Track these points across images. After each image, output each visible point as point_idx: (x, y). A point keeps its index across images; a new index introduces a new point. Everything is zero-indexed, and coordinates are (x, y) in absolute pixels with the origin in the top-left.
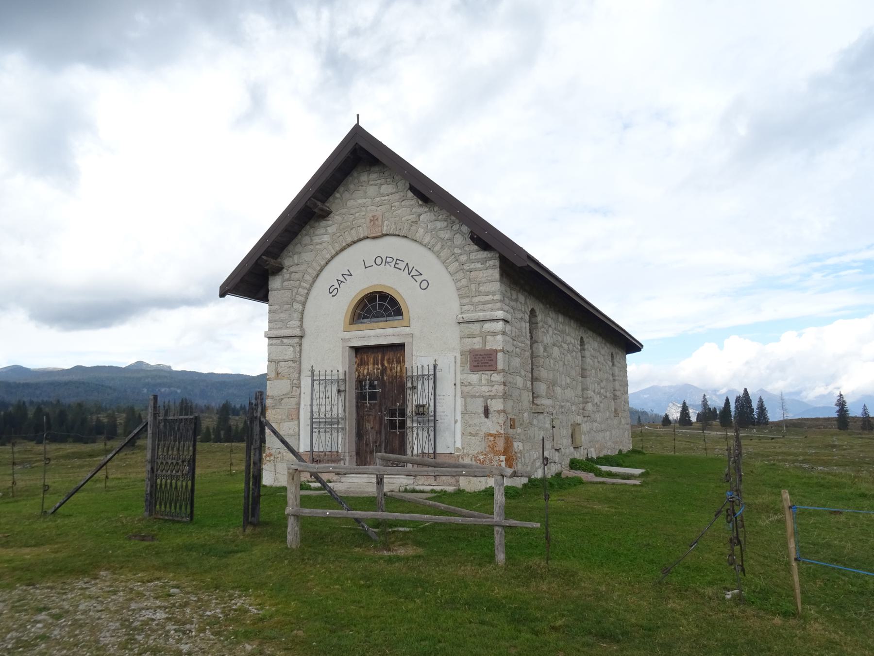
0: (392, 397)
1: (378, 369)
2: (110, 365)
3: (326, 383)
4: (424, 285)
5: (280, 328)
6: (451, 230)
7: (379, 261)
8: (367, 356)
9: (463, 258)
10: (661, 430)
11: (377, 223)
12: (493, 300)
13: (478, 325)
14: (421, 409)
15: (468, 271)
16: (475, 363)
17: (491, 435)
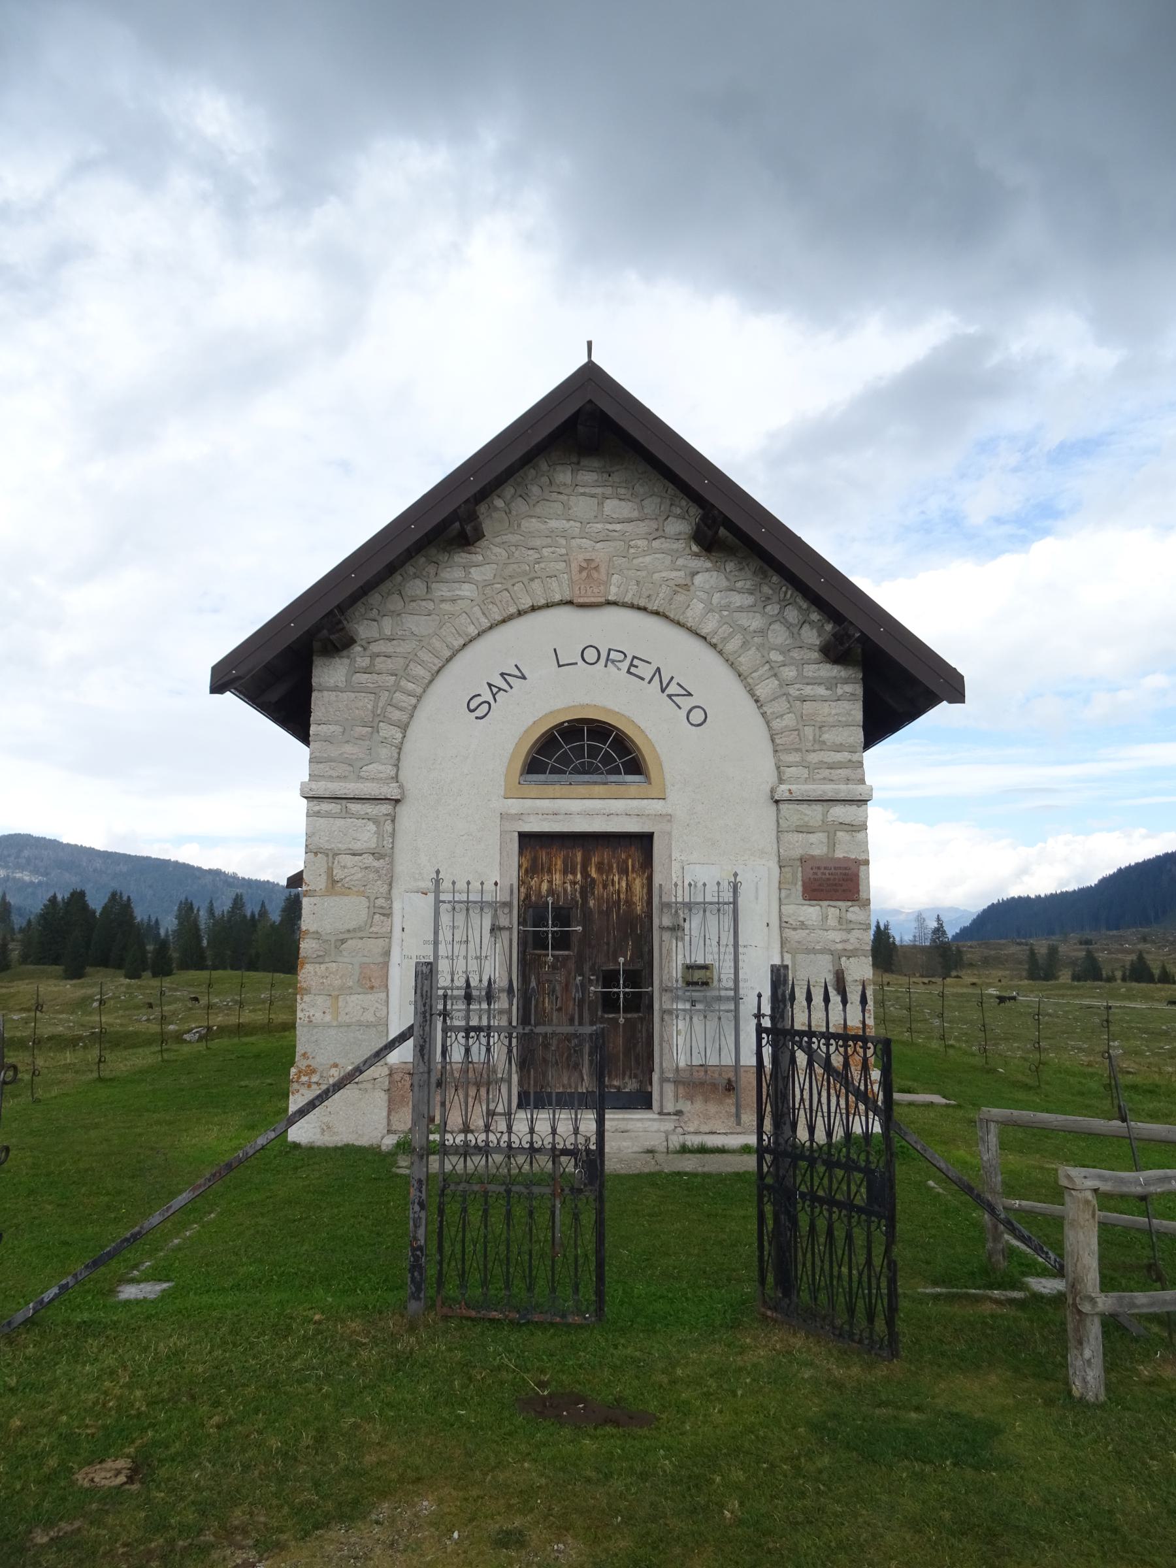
0: (608, 944)
1: (574, 883)
2: (985, 905)
3: (468, 910)
4: (697, 716)
6: (764, 614)
7: (591, 655)
8: (548, 854)
9: (789, 673)
11: (595, 575)
12: (850, 761)
13: (818, 808)
14: (698, 975)
15: (797, 699)
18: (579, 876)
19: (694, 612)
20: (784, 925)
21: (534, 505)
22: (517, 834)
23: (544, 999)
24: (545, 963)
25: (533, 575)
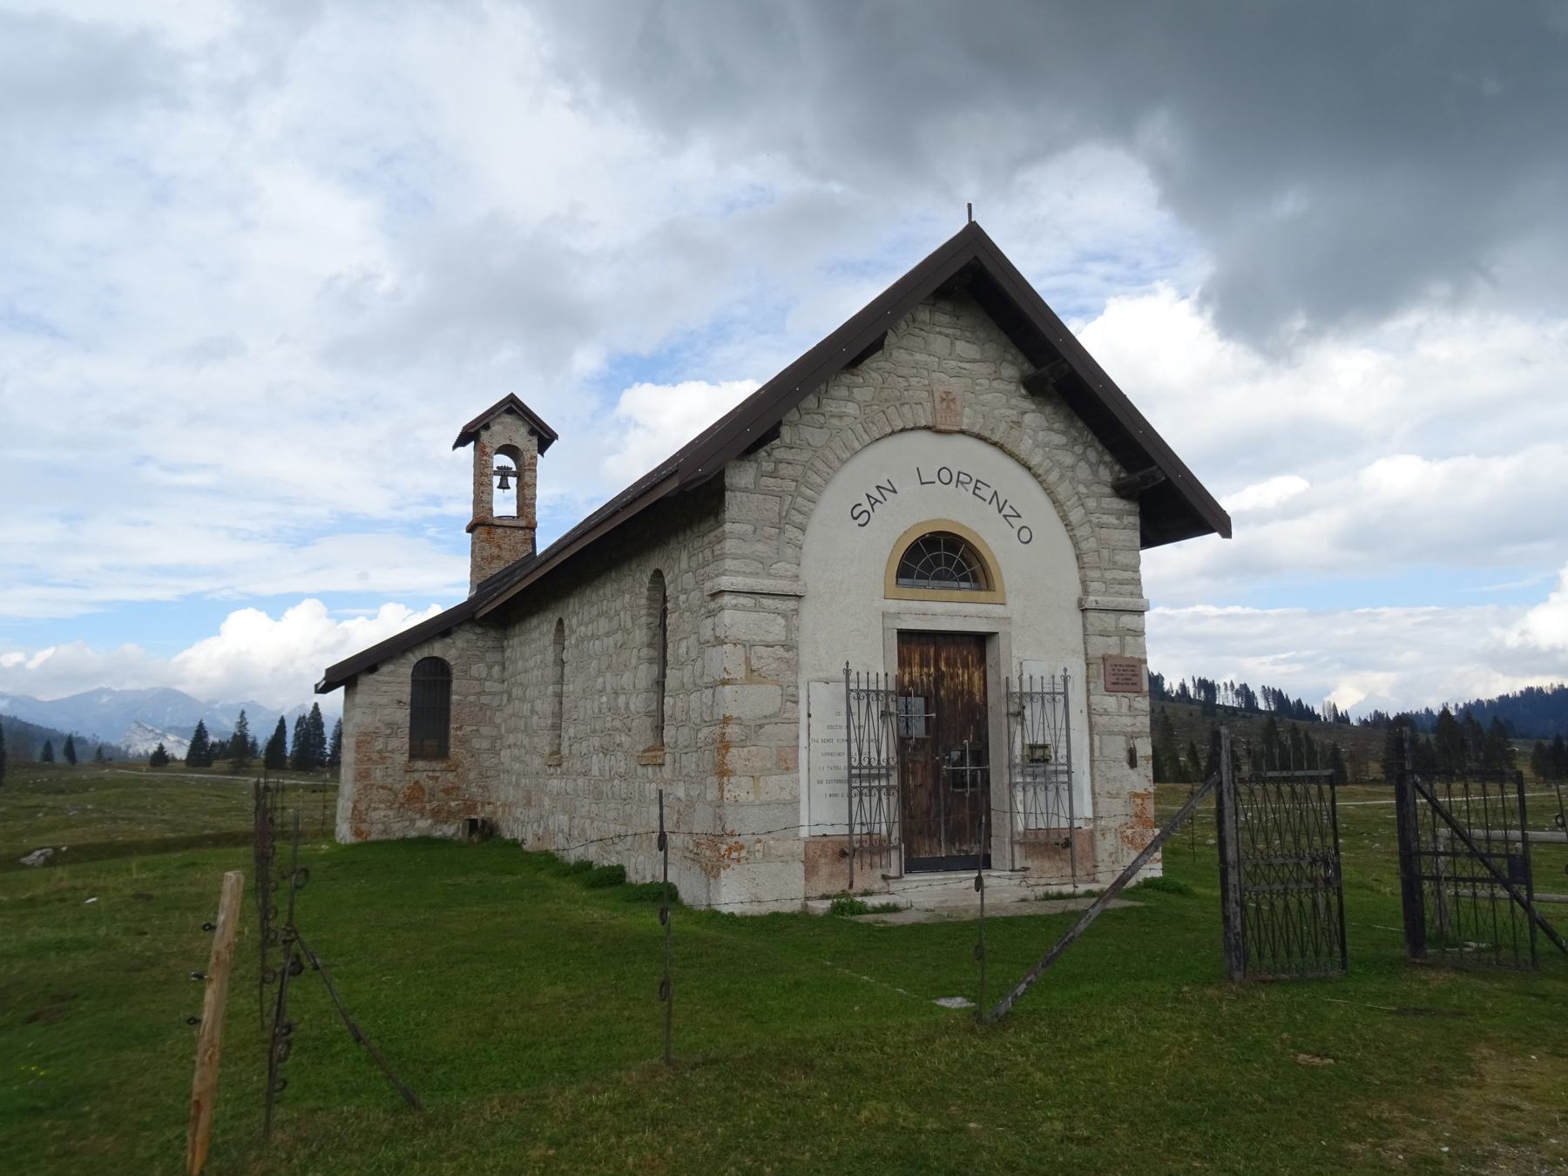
4: (1025, 535)
5: (755, 574)
6: (1073, 453)
7: (945, 476)
9: (1091, 503)
10: (145, 773)
11: (952, 406)
13: (1112, 617)
14: (1038, 754)
16: (1114, 679)
17: (1137, 795)
18: (932, 670)
19: (1025, 447)
20: (1093, 711)
21: (902, 338)
22: (896, 631)
23: (909, 776)
24: (909, 745)
25: (903, 400)
